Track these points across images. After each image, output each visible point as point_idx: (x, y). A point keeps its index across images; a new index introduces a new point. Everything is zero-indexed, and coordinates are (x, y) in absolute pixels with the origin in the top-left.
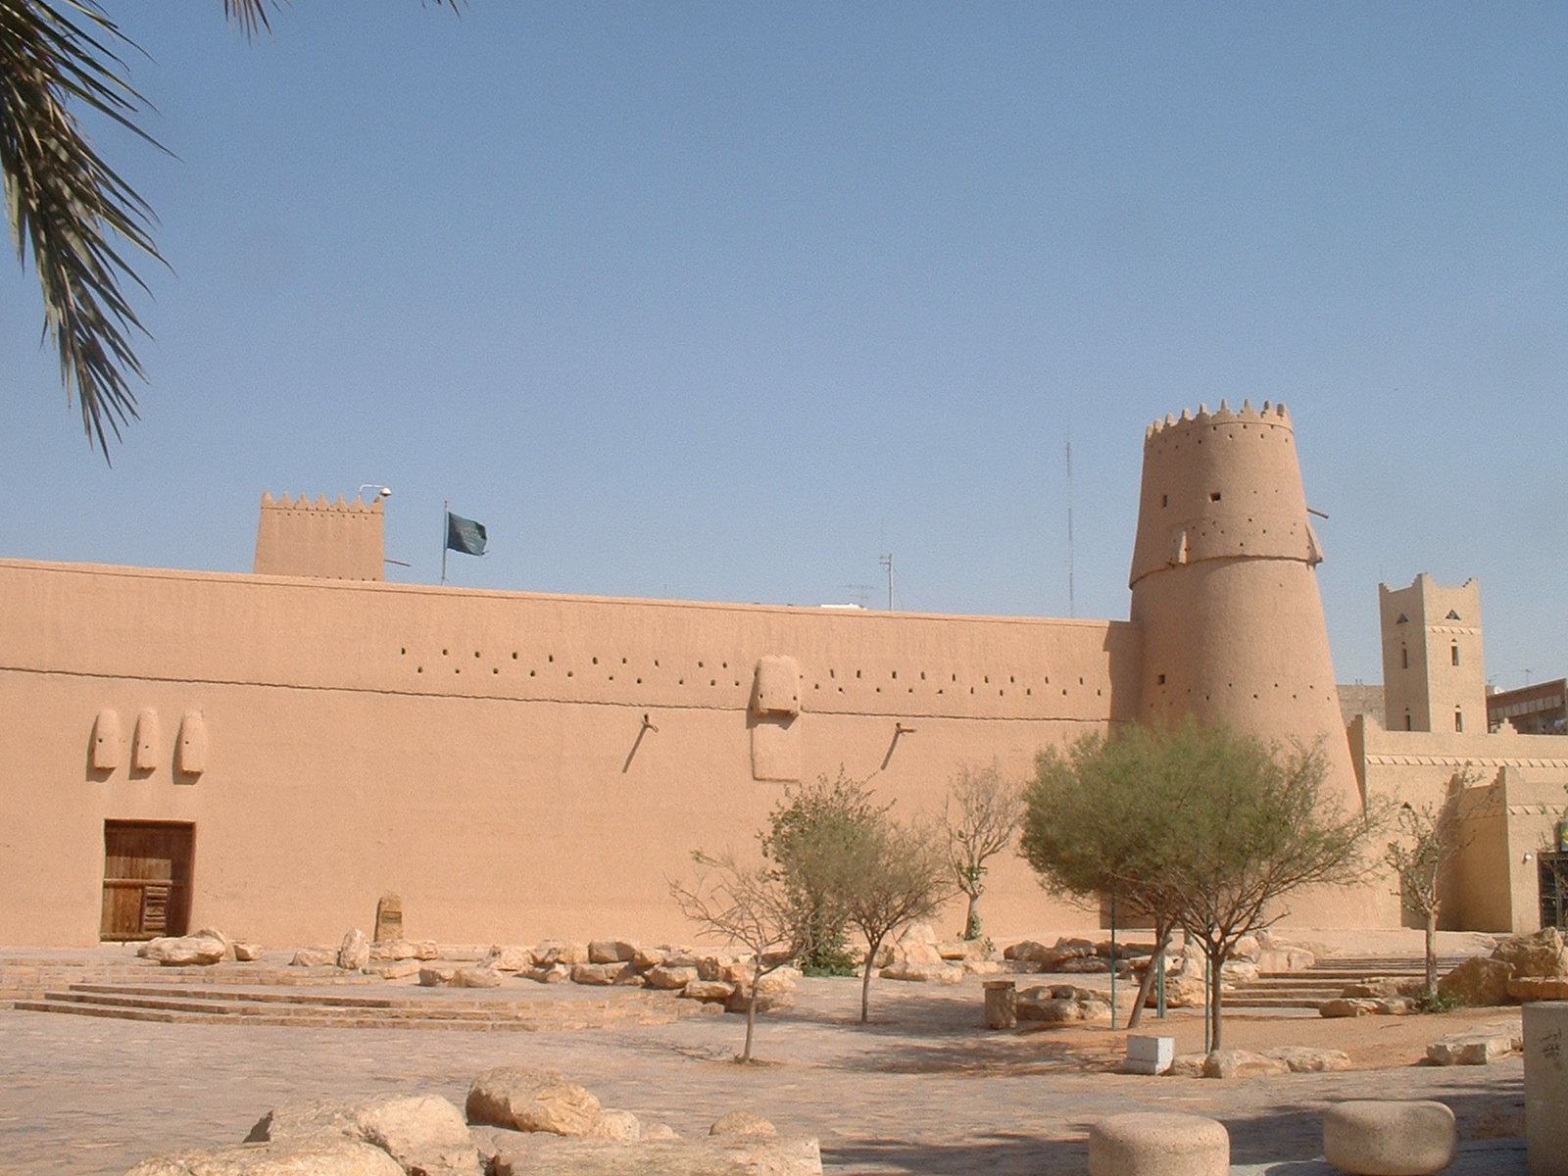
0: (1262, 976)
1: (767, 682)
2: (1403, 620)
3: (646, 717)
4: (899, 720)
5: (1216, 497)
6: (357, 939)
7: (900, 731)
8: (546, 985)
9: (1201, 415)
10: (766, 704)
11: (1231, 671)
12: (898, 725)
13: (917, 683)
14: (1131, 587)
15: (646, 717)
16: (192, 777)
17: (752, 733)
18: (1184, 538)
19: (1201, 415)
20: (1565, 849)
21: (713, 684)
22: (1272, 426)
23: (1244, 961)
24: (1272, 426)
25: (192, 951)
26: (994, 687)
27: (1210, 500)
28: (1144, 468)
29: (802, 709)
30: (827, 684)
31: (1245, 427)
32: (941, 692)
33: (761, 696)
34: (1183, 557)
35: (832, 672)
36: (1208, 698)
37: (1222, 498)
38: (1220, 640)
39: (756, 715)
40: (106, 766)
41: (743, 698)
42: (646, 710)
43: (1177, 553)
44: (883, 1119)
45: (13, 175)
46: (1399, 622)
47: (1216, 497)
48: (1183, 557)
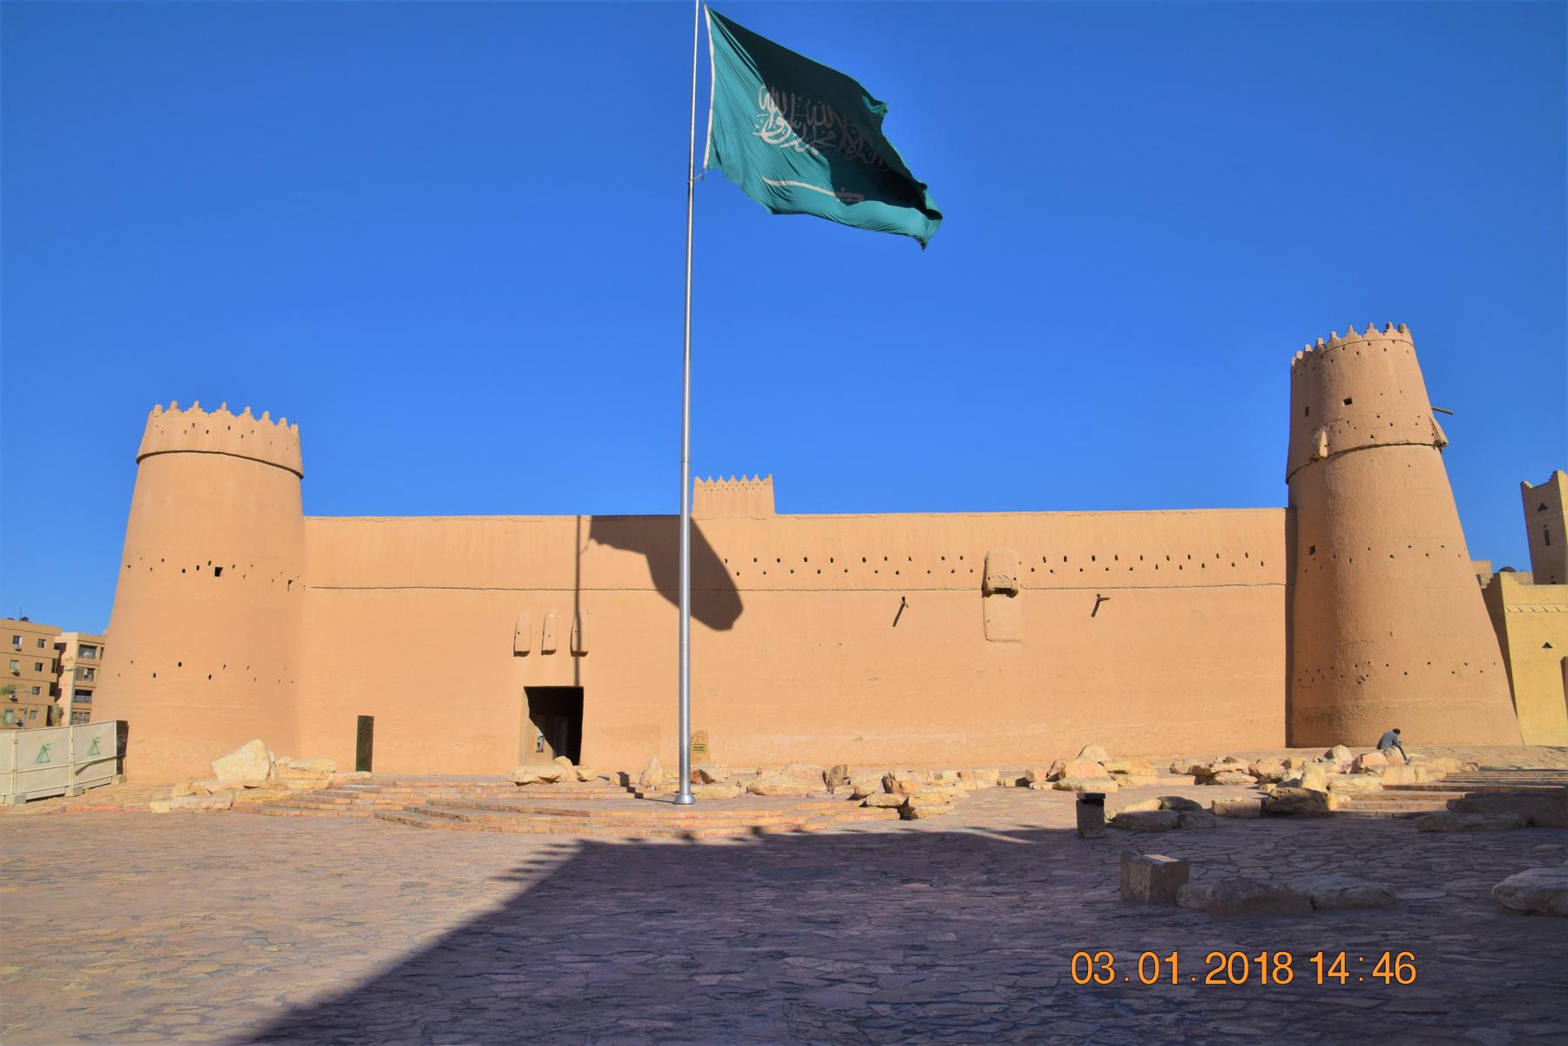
0: (1387, 787)
2: (1543, 507)
3: (904, 599)
4: (1099, 592)
5: (1348, 402)
6: (654, 764)
10: (992, 585)
11: (1368, 538)
12: (1098, 596)
14: (1287, 482)
15: (904, 599)
17: (984, 602)
20: (437, 1039)
22: (1394, 341)
23: (1369, 775)
24: (1394, 341)
26: (1175, 563)
27: (1343, 405)
28: (794, 53)
29: (1021, 586)
30: (1042, 569)
31: (1369, 344)
32: (1131, 569)
34: (1324, 452)
35: (1044, 558)
37: (1353, 401)
46: (1540, 510)
47: (1348, 402)
48: (1324, 452)
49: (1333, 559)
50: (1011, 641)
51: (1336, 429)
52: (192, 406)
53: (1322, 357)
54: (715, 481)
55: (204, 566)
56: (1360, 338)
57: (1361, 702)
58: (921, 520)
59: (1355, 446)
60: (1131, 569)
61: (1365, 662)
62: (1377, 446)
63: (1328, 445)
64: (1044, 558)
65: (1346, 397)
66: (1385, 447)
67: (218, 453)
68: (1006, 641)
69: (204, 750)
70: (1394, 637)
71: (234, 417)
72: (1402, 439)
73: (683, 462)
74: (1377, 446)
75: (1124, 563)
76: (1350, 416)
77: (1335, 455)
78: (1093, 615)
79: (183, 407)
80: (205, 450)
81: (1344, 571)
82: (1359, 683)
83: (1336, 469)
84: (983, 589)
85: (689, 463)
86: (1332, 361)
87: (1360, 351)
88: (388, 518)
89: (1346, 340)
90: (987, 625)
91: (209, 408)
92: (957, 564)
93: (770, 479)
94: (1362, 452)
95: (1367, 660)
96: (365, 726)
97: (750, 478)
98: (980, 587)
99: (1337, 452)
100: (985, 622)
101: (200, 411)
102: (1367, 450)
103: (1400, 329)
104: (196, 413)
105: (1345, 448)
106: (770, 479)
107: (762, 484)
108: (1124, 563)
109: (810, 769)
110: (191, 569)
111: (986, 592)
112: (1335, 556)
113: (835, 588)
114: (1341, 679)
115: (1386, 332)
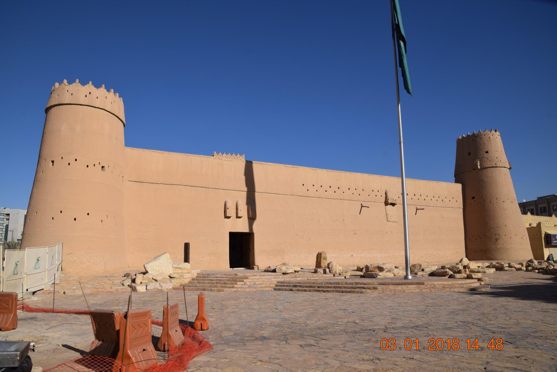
1: (389, 196)
3: (362, 204)
5: (487, 152)
7: (417, 209)
8: (276, 273)
9: (474, 134)
13: (426, 198)
15: (362, 204)
16: (229, 217)
17: (386, 207)
18: (478, 162)
19: (474, 134)
21: (376, 196)
25: (293, 270)
26: (416, 197)
27: (485, 153)
33: (388, 199)
34: (479, 167)
35: (421, 195)
36: (490, 202)
37: (489, 152)
38: (492, 188)
39: (386, 203)
40: (240, 216)
41: (383, 200)
42: (399, 201)
43: (478, 166)
44: (49, 283)
45: (397, 23)
48: (479, 167)
49: (483, 201)
50: (394, 222)
51: (483, 160)
52: (88, 83)
53: (476, 137)
54: (222, 154)
55: (97, 164)
56: (489, 133)
57: (497, 246)
58: (366, 176)
59: (490, 166)
60: (425, 200)
61: (498, 234)
62: (497, 167)
63: (480, 165)
64: (421, 195)
65: (486, 151)
66: (499, 168)
67: (102, 109)
68: (393, 222)
69: (102, 259)
70: (507, 226)
71: (107, 92)
72: (503, 166)
73: (400, 143)
74: (497, 167)
75: (418, 196)
76: (488, 157)
77: (483, 168)
78: (416, 214)
79: (70, 82)
80: (96, 107)
81: (488, 205)
82: (496, 240)
83: (483, 173)
84: (385, 203)
85: (403, 143)
86: (480, 139)
87: (490, 137)
88: (165, 152)
89: (485, 133)
90: (388, 216)
91: (98, 86)
92: (377, 194)
93: (244, 156)
94: (492, 168)
95: (499, 233)
96: (187, 246)
97: (236, 155)
98: (384, 202)
99: (484, 168)
100: (387, 215)
101: (93, 87)
102: (494, 168)
103: (496, 131)
104: (90, 87)
105: (487, 167)
106: (244, 156)
107: (241, 157)
108: (423, 198)
109: (392, 266)
110: (91, 166)
111: (386, 203)
112: (484, 200)
113: (340, 199)
114: (489, 239)
115: (491, 131)
